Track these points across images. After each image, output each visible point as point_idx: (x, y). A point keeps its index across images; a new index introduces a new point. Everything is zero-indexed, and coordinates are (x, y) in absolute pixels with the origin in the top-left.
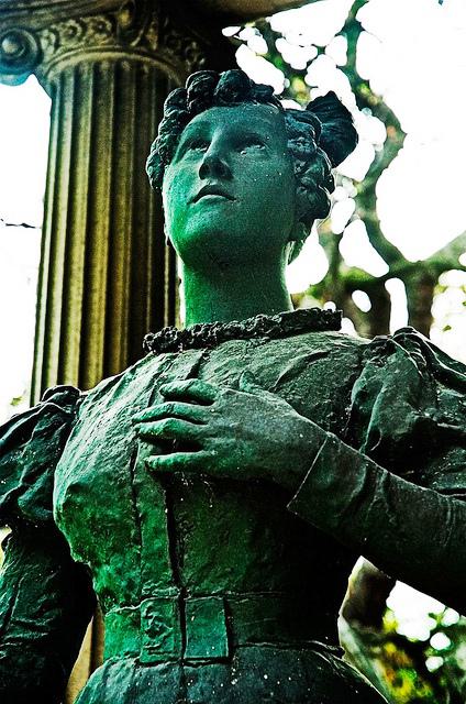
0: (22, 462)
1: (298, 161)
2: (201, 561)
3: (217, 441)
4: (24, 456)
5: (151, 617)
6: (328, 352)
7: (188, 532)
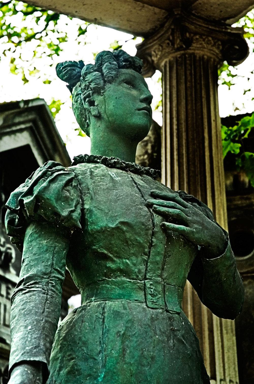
7: (169, 257)
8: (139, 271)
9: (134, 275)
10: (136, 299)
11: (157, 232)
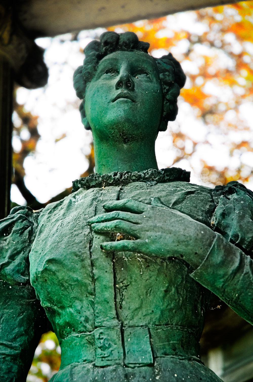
0: (7, 247)
1: (165, 86)
2: (134, 305)
3: (149, 233)
4: (8, 244)
5: (102, 338)
6: (195, 191)
8: (87, 320)
9: (80, 326)
10: (85, 359)
11: (97, 259)
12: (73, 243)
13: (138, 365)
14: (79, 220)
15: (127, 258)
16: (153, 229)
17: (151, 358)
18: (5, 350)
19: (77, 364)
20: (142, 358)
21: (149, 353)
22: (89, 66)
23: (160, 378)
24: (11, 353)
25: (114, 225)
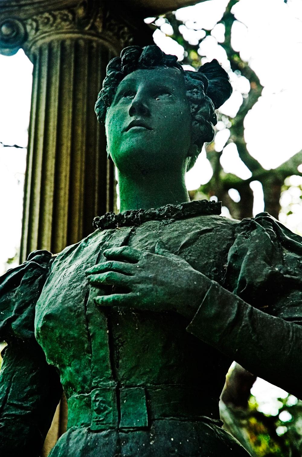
1: (193, 105)
2: (130, 365)
4: (16, 296)
5: (98, 401)
7: (122, 345)
11: (91, 314)
12: (69, 297)
13: (132, 429)
14: (80, 270)
15: (122, 313)
16: (145, 281)
17: (146, 422)
18: (15, 411)
19: (76, 427)
20: (137, 421)
21: (145, 415)
22: (108, 89)
23: (154, 443)
24: (21, 413)
25: (105, 277)
